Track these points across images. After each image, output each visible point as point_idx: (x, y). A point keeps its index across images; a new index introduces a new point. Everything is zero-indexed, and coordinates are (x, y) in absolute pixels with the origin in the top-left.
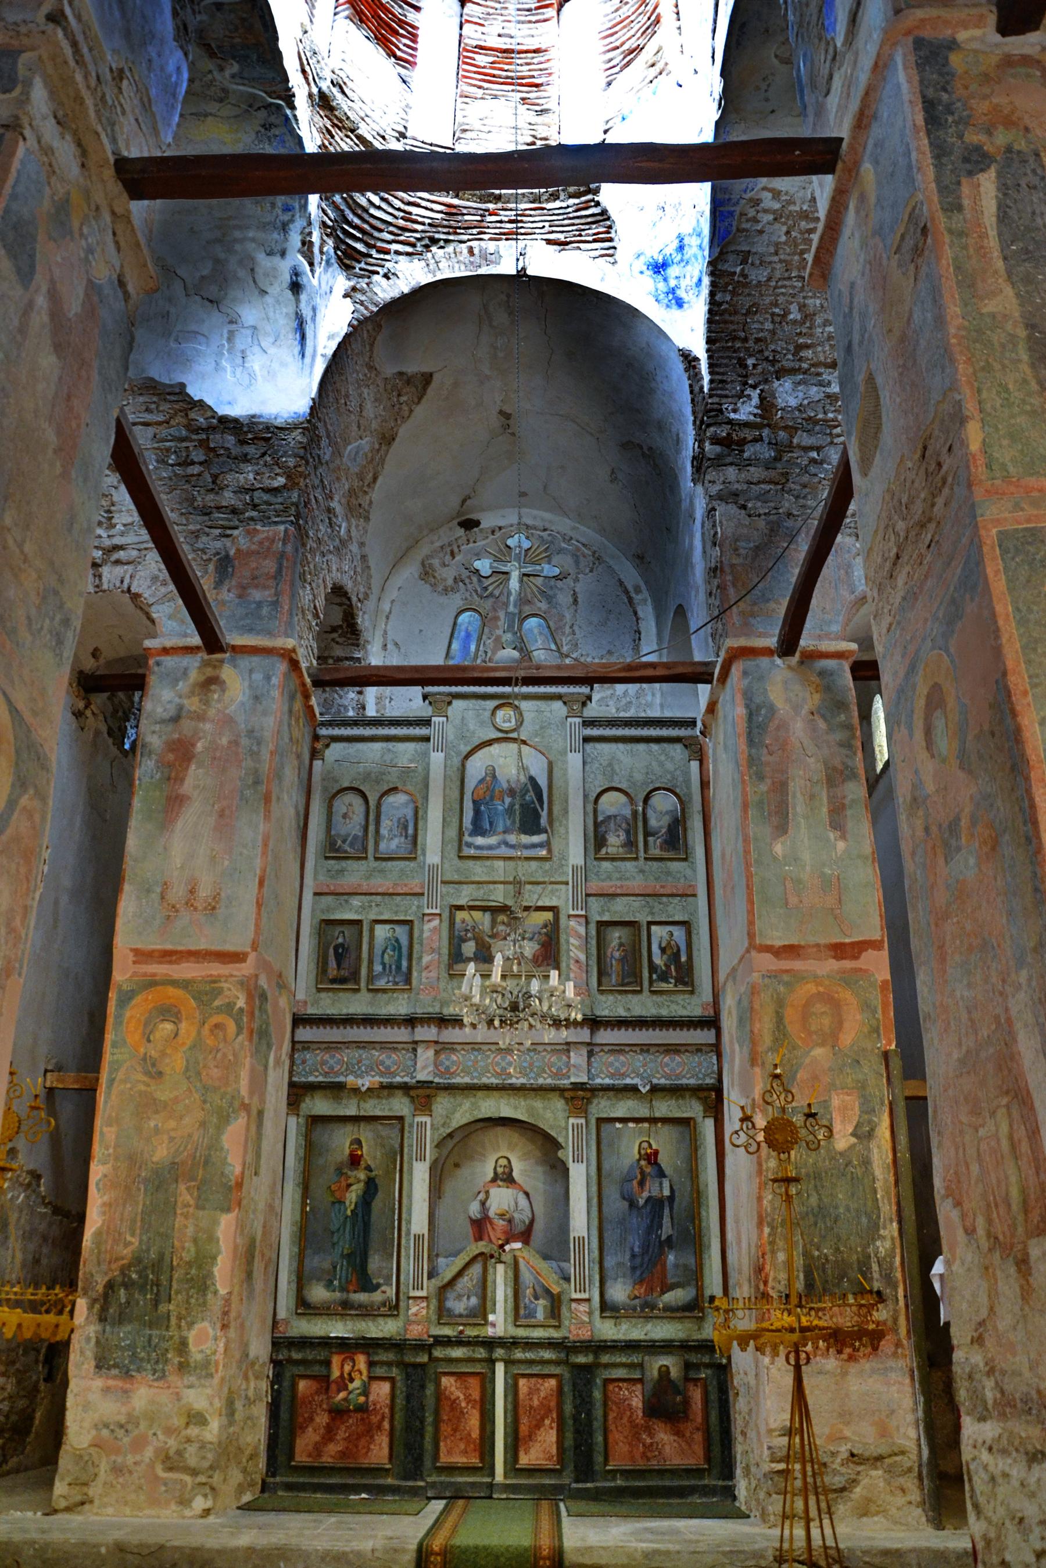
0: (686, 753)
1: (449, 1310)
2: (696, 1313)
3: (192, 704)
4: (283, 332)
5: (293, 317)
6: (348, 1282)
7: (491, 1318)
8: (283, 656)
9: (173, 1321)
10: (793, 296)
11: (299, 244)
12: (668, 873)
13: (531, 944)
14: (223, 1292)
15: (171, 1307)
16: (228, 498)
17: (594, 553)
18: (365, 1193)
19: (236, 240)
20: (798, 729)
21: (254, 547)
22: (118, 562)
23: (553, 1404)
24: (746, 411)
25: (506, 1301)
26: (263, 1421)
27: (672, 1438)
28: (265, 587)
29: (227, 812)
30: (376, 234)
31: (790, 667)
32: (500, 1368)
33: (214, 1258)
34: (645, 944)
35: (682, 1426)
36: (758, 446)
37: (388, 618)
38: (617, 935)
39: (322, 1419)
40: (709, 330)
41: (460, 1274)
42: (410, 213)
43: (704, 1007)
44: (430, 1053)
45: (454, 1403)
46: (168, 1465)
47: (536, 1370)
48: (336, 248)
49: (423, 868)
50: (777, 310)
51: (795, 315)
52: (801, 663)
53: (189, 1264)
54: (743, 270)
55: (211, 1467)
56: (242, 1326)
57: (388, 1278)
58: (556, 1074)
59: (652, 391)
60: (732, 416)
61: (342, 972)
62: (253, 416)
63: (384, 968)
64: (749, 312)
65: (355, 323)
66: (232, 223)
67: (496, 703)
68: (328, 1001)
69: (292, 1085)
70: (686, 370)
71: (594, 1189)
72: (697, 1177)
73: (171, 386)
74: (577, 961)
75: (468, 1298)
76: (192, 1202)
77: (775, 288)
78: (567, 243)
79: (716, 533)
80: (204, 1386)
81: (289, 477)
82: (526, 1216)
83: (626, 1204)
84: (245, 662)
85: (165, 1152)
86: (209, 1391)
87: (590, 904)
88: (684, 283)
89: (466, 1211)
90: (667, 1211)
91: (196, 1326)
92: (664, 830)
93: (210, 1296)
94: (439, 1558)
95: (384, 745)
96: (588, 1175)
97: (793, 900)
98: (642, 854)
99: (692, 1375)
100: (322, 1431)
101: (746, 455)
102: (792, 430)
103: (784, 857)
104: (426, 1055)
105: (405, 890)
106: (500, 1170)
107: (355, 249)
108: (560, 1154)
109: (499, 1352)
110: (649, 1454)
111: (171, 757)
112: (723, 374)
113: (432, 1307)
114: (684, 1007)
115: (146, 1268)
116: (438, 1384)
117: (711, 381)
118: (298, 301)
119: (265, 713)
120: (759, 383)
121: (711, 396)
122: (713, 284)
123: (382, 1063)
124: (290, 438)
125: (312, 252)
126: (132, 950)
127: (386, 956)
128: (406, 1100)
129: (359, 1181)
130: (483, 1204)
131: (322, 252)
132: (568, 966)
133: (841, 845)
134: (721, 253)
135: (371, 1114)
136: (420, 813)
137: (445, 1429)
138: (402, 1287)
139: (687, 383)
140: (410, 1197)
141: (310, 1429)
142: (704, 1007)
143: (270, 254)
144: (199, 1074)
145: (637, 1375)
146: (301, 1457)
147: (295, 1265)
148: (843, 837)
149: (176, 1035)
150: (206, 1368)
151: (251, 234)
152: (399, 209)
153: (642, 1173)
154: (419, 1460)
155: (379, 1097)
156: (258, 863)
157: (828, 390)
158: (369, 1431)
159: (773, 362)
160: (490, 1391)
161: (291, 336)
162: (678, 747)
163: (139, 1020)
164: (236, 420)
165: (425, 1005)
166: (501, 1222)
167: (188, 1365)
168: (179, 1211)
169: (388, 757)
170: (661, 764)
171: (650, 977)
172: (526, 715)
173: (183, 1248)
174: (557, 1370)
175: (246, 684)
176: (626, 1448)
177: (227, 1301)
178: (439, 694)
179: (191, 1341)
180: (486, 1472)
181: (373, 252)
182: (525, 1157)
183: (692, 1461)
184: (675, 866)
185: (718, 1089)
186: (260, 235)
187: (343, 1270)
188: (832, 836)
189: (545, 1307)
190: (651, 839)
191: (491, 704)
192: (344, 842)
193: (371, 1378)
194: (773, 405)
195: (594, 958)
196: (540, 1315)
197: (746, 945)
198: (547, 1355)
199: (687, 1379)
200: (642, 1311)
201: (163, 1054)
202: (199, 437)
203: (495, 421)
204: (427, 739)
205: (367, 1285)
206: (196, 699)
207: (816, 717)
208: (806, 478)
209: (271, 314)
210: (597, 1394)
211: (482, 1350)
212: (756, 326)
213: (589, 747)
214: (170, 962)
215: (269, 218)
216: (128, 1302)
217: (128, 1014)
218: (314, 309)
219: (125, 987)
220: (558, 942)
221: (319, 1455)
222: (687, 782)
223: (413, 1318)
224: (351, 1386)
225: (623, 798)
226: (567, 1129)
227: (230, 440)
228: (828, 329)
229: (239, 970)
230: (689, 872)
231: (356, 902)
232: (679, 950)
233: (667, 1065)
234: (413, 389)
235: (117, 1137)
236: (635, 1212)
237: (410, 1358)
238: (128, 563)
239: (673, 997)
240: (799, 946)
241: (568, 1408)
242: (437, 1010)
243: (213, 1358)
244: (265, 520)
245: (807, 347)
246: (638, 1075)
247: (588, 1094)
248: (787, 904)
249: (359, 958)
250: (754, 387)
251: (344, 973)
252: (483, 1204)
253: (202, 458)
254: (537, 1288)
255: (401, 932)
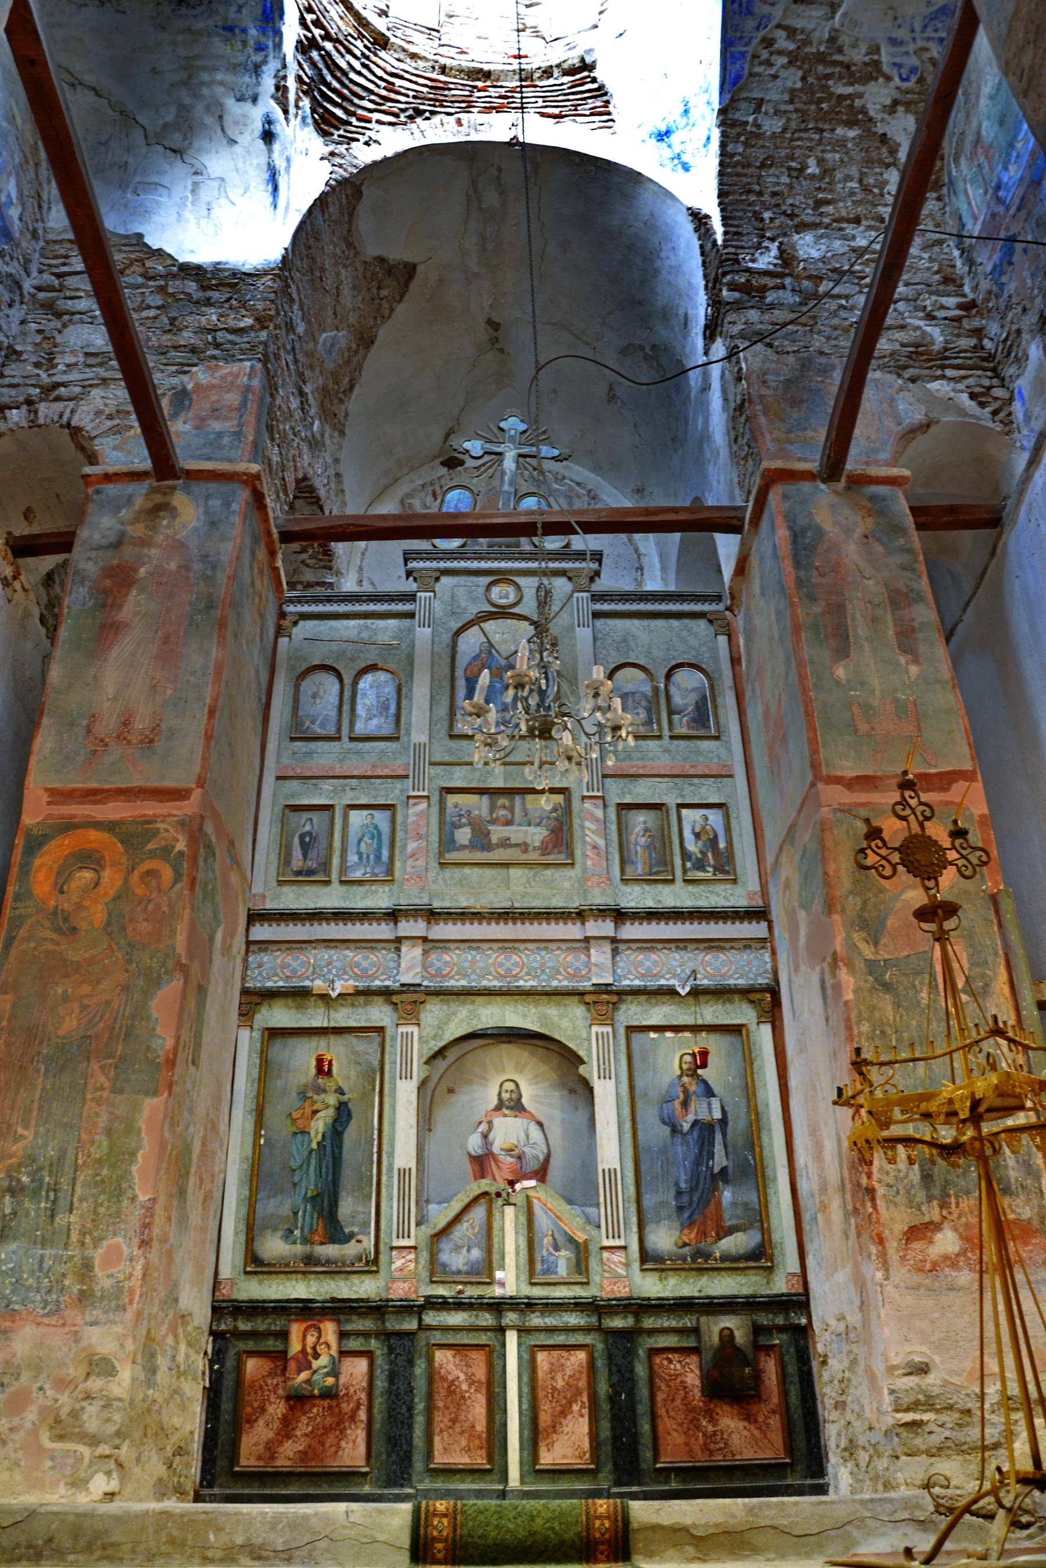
0: (711, 630)
1: (444, 1265)
2: (763, 1263)
3: (138, 530)
4: (253, 184)
5: (265, 167)
6: (312, 1232)
7: (499, 1275)
8: (245, 482)
9: (74, 1237)
10: (811, 149)
11: (273, 89)
12: (699, 753)
13: (538, 830)
14: (142, 1198)
15: (72, 1219)
16: (187, 337)
17: (589, 491)
18: (335, 1121)
19: (202, 84)
20: (852, 552)
21: (214, 382)
22: (58, 399)
23: (583, 1383)
24: (766, 260)
25: (517, 1253)
26: (197, 1409)
27: (741, 1424)
28: (226, 419)
29: (173, 639)
30: (356, 101)
31: (835, 492)
32: (512, 1339)
33: (133, 1154)
34: (675, 829)
35: (754, 1408)
36: (781, 292)
37: (363, 554)
38: (642, 819)
39: (277, 1409)
40: (721, 183)
41: (457, 1219)
42: (393, 84)
43: (751, 895)
44: (418, 951)
45: (452, 1388)
46: (58, 1431)
47: (560, 1339)
48: (313, 111)
49: (407, 749)
50: (794, 164)
51: (813, 169)
52: (848, 488)
53: (99, 1162)
54: (756, 119)
55: (118, 1434)
56: (170, 1255)
57: (366, 1225)
58: (574, 976)
59: (656, 272)
60: (750, 265)
61: (309, 863)
62: (219, 263)
63: (360, 858)
64: (763, 166)
65: (333, 183)
66: (199, 63)
67: (490, 579)
68: (291, 895)
69: (245, 992)
70: (696, 230)
71: (626, 1111)
72: (754, 1094)
73: (127, 237)
74: (595, 847)
75: (469, 1250)
76: (106, 1084)
77: (792, 140)
78: (563, 117)
79: (741, 369)
80: (113, 1322)
81: (257, 319)
82: (540, 1152)
83: (667, 1130)
84: (200, 488)
85: (75, 1023)
86: (119, 1329)
87: (607, 785)
88: (689, 147)
89: (463, 1146)
90: (718, 1137)
91: (105, 1243)
92: (691, 708)
93: (125, 1203)
94: (445, 1521)
95: (362, 622)
96: (617, 1094)
97: (863, 727)
98: (666, 733)
99: (763, 1340)
100: (277, 1424)
101: (768, 300)
102: (818, 279)
103: (848, 681)
104: (412, 954)
105: (386, 772)
106: (505, 1096)
107: (333, 114)
108: (582, 1070)
109: (510, 1317)
110: (712, 1446)
111: (108, 582)
112: (738, 226)
113: (422, 1261)
114: (726, 898)
115: (41, 1168)
116: (430, 1360)
117: (725, 233)
118: (270, 151)
119: (223, 538)
120: (778, 236)
121: (725, 247)
122: (724, 135)
123: (358, 965)
124: (259, 284)
125: (287, 98)
126: (47, 790)
127: (363, 844)
128: (387, 1009)
129: (327, 1107)
130: (485, 1136)
131: (297, 107)
132: (585, 855)
133: (914, 670)
134: (733, 100)
135: (344, 1025)
136: (404, 691)
137: (441, 1420)
138: (382, 1235)
139: (696, 243)
140: (393, 1124)
141: (261, 1423)
142: (751, 895)
143: (240, 99)
144: (124, 928)
145: (691, 1343)
146: (247, 1460)
147: (244, 1211)
148: (916, 661)
149: (97, 884)
150: (117, 1298)
151: (219, 76)
152: (381, 78)
153: (686, 1091)
154: (406, 1459)
155: (353, 1005)
156: (208, 692)
157: (853, 244)
158: (340, 1424)
159: (792, 216)
160: (499, 1369)
161: (262, 187)
162: (702, 623)
163: (51, 868)
164: (199, 268)
165: (411, 896)
166: (510, 1160)
167: (92, 1294)
168: (89, 1096)
169: (365, 635)
170: (683, 640)
171: (684, 865)
172: (525, 591)
173: (93, 1142)
174: (587, 1340)
175: (201, 510)
176: (680, 1439)
177: (149, 1210)
178: (425, 569)
179: (97, 1262)
180: (496, 1477)
181: (353, 120)
182: (536, 1079)
183: (769, 1454)
184: (705, 745)
185: (774, 991)
186: (229, 78)
187: (306, 1216)
188: (902, 660)
189: (568, 1259)
190: (676, 717)
191: (485, 580)
192: (313, 722)
193: (343, 1353)
194: (794, 258)
195: (615, 844)
196: (563, 1270)
197: (810, 778)
198: (573, 1319)
199: (757, 1347)
200: (694, 1261)
201: (79, 907)
202: (157, 283)
203: (482, 334)
204: (411, 615)
205: (336, 1234)
206: (141, 526)
207: (871, 540)
208: (836, 321)
209: (240, 165)
210: (641, 1370)
211: (487, 1315)
212: (770, 179)
213: (600, 623)
214: (95, 803)
215: (241, 58)
216: (14, 1213)
217: (37, 862)
218: (288, 160)
219: (35, 831)
220: (571, 827)
221: (273, 1458)
222: (715, 658)
223: (397, 1274)
224: (315, 1364)
225: (641, 675)
226: (589, 1040)
227: (191, 286)
228: (849, 184)
229: (180, 808)
230: (723, 752)
231: (327, 785)
232: (716, 836)
233: (710, 964)
234: (395, 283)
235: (13, 1007)
236: (678, 1140)
237: (393, 1324)
238: (70, 399)
239: (712, 888)
240: (875, 777)
241: (603, 1388)
242: (426, 901)
243: (127, 1284)
244: (230, 358)
245: (828, 202)
246: (674, 976)
247: (615, 998)
248: (856, 731)
249: (330, 846)
250: (772, 240)
251: (311, 864)
252: (485, 1136)
253: (160, 303)
254: (557, 1236)
255: (381, 818)
